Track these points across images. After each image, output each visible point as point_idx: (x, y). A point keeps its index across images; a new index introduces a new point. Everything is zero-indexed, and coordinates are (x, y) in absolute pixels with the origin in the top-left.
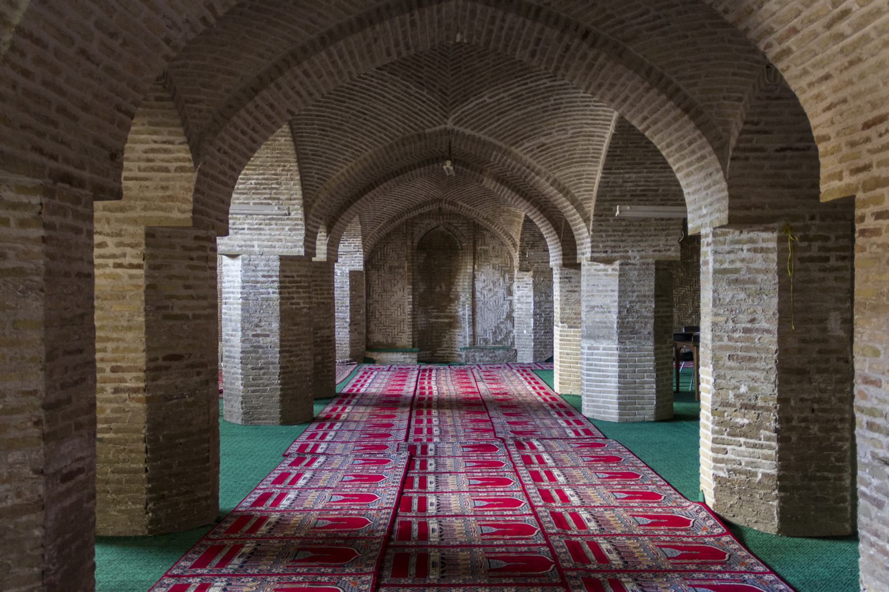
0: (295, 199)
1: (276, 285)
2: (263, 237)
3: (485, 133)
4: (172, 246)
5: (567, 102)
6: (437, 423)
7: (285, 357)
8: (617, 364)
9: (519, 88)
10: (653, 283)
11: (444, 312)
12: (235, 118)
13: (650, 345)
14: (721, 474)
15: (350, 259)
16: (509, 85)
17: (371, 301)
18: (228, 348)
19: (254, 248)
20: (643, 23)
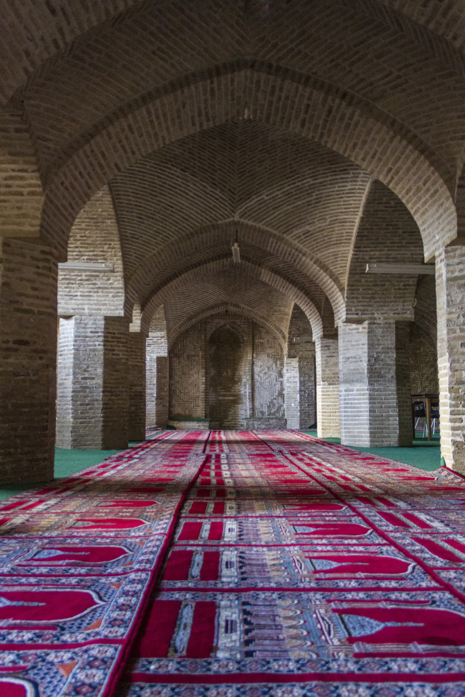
0: (117, 272)
1: (101, 339)
2: (92, 302)
3: (264, 224)
4: (23, 256)
5: (325, 196)
6: (227, 468)
7: (107, 396)
8: (368, 401)
9: (289, 187)
10: (394, 339)
11: (229, 391)
12: (75, 157)
13: (393, 387)
14: (458, 439)
15: (156, 347)
16: (281, 185)
17: (173, 382)
18: (62, 390)
19: (86, 301)
20: (389, 82)
